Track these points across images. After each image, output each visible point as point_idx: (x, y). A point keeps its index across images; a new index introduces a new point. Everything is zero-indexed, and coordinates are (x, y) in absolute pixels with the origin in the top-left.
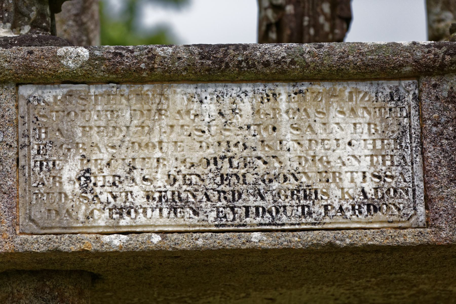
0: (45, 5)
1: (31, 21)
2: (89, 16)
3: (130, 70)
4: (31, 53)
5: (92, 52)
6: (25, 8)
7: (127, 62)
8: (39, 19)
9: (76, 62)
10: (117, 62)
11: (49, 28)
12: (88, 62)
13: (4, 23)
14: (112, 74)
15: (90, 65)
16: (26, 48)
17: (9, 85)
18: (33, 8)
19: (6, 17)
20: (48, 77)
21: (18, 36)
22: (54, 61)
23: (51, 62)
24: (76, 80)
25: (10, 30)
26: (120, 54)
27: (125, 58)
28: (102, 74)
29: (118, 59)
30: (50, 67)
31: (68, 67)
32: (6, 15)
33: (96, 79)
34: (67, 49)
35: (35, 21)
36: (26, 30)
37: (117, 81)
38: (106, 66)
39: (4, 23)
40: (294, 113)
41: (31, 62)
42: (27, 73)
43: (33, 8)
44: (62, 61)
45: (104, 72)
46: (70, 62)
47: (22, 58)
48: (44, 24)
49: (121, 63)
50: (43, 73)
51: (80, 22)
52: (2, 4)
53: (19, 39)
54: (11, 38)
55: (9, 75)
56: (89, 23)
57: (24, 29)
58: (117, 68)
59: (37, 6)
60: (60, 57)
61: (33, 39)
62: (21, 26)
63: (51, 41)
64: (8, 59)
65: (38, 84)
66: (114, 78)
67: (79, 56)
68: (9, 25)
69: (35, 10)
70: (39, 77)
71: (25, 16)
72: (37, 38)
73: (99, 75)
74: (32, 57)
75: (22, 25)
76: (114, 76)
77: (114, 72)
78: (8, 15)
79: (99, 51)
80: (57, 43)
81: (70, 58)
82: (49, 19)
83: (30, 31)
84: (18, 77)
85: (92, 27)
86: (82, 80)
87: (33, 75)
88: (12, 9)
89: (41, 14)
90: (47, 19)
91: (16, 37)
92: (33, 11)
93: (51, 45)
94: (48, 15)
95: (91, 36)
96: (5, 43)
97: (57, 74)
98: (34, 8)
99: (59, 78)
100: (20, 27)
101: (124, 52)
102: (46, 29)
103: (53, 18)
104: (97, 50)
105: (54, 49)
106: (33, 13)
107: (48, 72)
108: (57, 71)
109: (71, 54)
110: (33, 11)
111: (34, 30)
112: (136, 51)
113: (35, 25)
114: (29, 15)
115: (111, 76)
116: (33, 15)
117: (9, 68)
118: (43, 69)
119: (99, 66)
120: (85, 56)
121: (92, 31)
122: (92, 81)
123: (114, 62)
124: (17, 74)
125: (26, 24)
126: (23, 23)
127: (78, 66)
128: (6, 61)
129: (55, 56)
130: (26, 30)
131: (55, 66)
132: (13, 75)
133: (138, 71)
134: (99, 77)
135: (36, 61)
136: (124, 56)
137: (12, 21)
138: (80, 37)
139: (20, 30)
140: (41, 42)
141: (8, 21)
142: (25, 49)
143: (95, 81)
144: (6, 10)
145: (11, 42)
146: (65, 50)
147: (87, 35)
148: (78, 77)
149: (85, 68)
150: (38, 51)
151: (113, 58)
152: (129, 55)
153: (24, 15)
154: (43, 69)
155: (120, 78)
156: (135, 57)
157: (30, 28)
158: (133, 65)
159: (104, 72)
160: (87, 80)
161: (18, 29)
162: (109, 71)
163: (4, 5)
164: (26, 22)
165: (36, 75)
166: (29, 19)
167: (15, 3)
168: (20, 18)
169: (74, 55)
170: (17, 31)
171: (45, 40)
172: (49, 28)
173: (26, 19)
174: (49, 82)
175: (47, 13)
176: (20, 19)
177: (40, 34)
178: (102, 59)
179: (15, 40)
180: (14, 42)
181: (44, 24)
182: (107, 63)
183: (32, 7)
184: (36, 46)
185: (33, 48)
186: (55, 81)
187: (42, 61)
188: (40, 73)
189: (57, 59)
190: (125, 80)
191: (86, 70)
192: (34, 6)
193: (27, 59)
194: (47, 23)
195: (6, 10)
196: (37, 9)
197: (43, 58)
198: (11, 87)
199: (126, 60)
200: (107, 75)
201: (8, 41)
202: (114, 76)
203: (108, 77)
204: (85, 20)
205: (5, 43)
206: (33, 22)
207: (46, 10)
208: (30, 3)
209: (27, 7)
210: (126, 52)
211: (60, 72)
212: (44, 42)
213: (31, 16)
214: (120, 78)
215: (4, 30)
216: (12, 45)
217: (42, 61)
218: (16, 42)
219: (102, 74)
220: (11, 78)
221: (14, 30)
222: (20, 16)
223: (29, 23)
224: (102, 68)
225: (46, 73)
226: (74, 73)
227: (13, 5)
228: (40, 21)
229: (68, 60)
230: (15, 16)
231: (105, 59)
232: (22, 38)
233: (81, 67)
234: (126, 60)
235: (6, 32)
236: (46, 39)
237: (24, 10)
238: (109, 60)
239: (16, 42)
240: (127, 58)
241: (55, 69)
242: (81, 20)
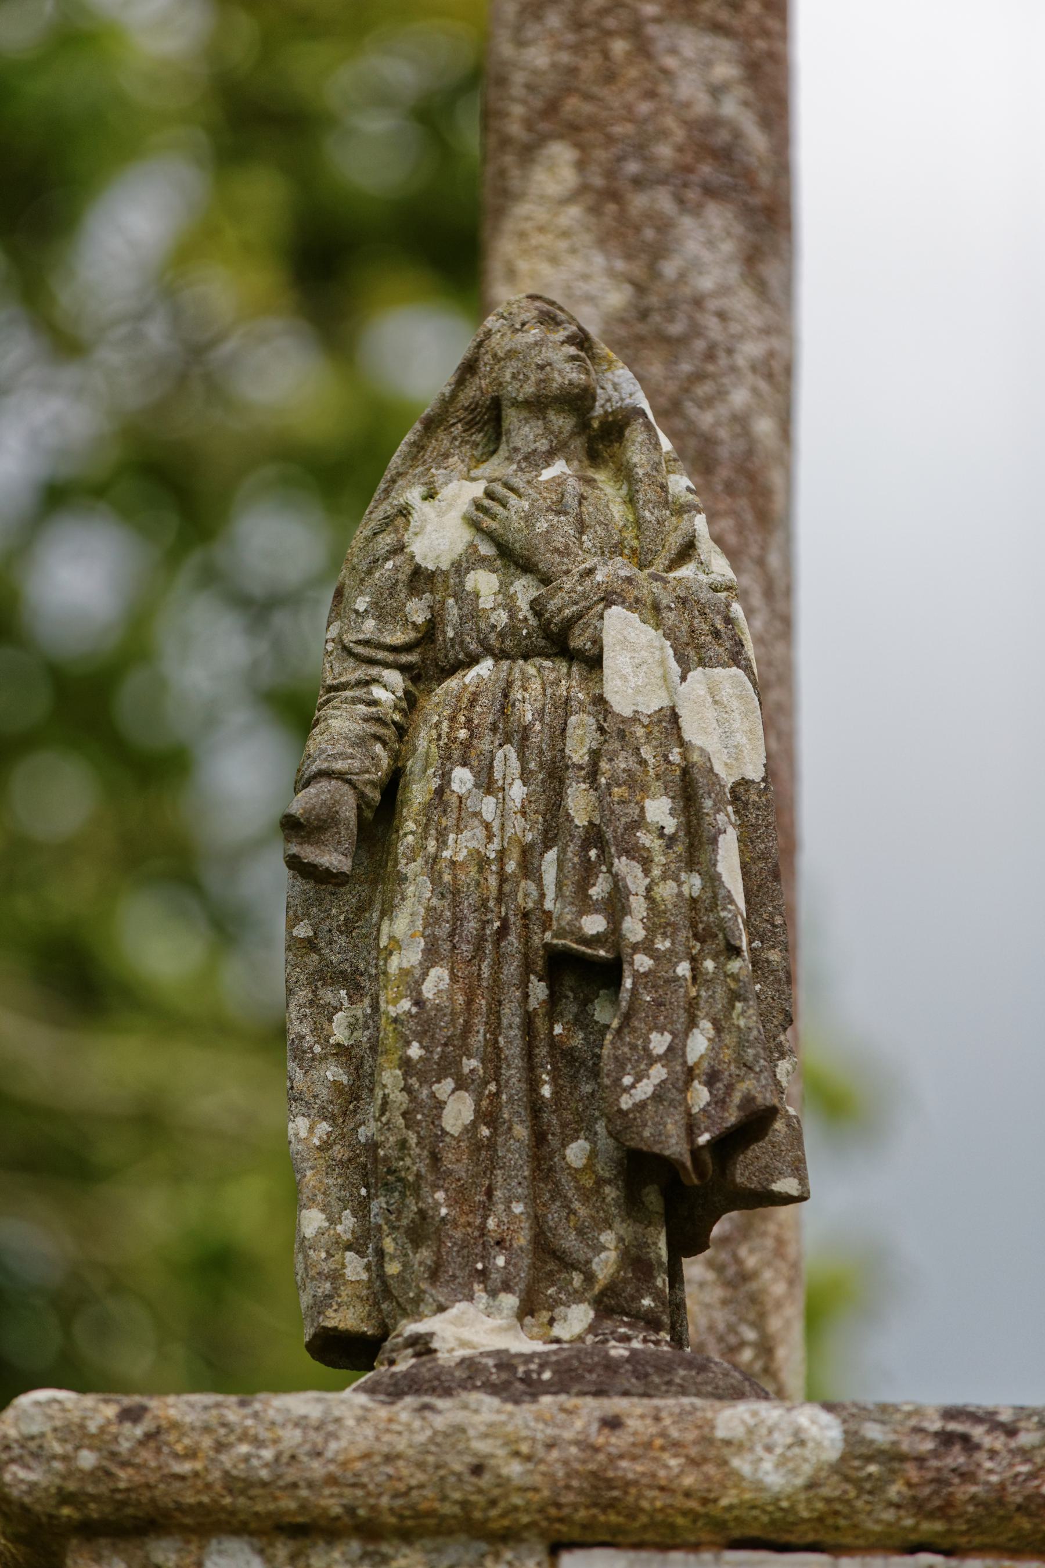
0: (650, 1224)
1: (597, 1289)
2: (770, 1243)
3: (1001, 1502)
4: (612, 1423)
5: (852, 1426)
6: (573, 1236)
7: (993, 1472)
8: (625, 1281)
9: (791, 1465)
10: (954, 1470)
11: (665, 1319)
12: (840, 1469)
13: (493, 1294)
14: (931, 1516)
15: (847, 1479)
16: (590, 1401)
17: (523, 1548)
18: (603, 1238)
19: (498, 1269)
20: (680, 1521)
21: (555, 1352)
22: (705, 1460)
23: (694, 1463)
24: (792, 1538)
25: (515, 1321)
26: (965, 1439)
27: (981, 1456)
28: (889, 1515)
29: (957, 1458)
30: (688, 1481)
31: (759, 1487)
32: (501, 1261)
33: (867, 1533)
34: (755, 1414)
35: (611, 1289)
36: (576, 1320)
37: (946, 1543)
38: (909, 1485)
39: (493, 1294)
40: (438, 455)
41: (612, 1459)
42: (595, 1505)
43: (603, 1238)
44: (736, 1462)
45: (898, 1506)
46: (767, 1465)
47: (577, 1443)
48: (647, 1302)
49: (967, 1476)
50: (659, 1504)
51: (731, 1271)
52: (485, 1218)
53: (557, 1362)
54: (528, 1358)
55: (527, 1511)
56: (767, 1274)
57: (565, 1319)
58: (951, 1494)
59: (621, 1228)
60: (728, 1443)
61: (611, 1366)
62: (553, 1304)
63: (682, 1372)
64: (524, 1448)
65: (638, 1546)
66: (937, 1534)
67: (802, 1443)
68: (510, 1301)
69: (612, 1246)
70: (644, 1519)
71: (573, 1267)
72: (628, 1360)
73: (878, 1521)
74: (618, 1441)
75: (558, 1302)
76: (939, 1526)
77: (940, 1508)
78: (507, 1262)
79: (883, 1423)
80: (706, 1383)
81: (769, 1449)
82: (661, 1281)
83: (592, 1329)
84: (561, 1520)
85: (779, 1289)
86: (811, 1537)
87: (618, 1513)
88: (522, 1240)
89: (636, 1262)
90: (659, 1283)
91: (547, 1354)
92: (604, 1248)
93: (684, 1392)
94: (661, 1264)
95: (775, 1324)
96: (504, 1376)
97: (713, 1510)
98: (608, 1238)
99: (718, 1525)
100: (551, 1309)
101: (977, 1432)
102: (652, 1323)
103: (676, 1277)
104: (875, 1421)
105: (703, 1410)
106: (603, 1255)
107: (679, 1501)
108: (715, 1501)
109: (770, 1432)
110: (604, 1248)
111: (608, 1324)
112: (1028, 1430)
113: (610, 1305)
114: (589, 1262)
115: (926, 1526)
116: (605, 1264)
117: (528, 1481)
118: (662, 1489)
119: (875, 1487)
120: (826, 1443)
121: (779, 1305)
122: (848, 1540)
123: (939, 1470)
124: (558, 1506)
125: (577, 1297)
126: (563, 1296)
127: (799, 1481)
128: (517, 1454)
129: (707, 1440)
130: (576, 1320)
131: (708, 1478)
132: (541, 1510)
133: (1033, 1507)
134: (878, 1528)
135: (634, 1458)
136: (978, 1447)
137: (522, 1286)
138: (732, 1329)
139: (552, 1321)
140: (646, 1377)
141: (507, 1287)
142: (590, 1409)
143: (861, 1542)
144: (498, 1243)
145: (528, 1373)
146: (747, 1417)
147: (759, 1323)
148: (794, 1524)
149: (826, 1491)
150: (642, 1417)
151: (935, 1454)
152: (998, 1445)
153: (566, 1262)
154: (662, 1489)
155: (963, 1533)
156: (1025, 1454)
157: (592, 1314)
158: (1014, 1484)
159: (898, 1506)
160: (829, 1538)
161: (545, 1316)
162: (917, 1506)
163: (491, 1223)
164: (576, 1291)
165: (632, 1513)
166: (590, 1278)
167: (536, 1217)
168: (551, 1273)
169: (782, 1439)
170: (542, 1325)
171: (660, 1370)
172: (665, 1319)
173: (577, 1279)
174: (678, 1541)
175: (660, 1257)
176: (550, 1278)
177: (636, 1344)
178: (892, 1457)
179: (542, 1367)
180: (539, 1374)
181: (647, 1302)
182: (912, 1472)
183: (601, 1230)
184: (626, 1394)
185: (617, 1404)
186: (705, 1537)
187: (655, 1459)
188: (645, 1504)
189: (710, 1451)
190: (977, 1540)
191: (828, 1501)
192: (610, 1227)
193: (596, 1449)
194: (657, 1296)
195: (498, 1243)
196: (621, 1239)
197: (663, 1449)
198: (531, 1556)
199: (988, 1465)
200: (909, 1522)
201: (513, 1368)
202: (939, 1526)
203: (914, 1529)
204: (751, 1262)
205: (504, 1376)
206: (603, 1293)
207: (655, 1244)
208: (592, 1217)
209: (580, 1232)
210: (989, 1432)
211: (724, 1502)
212: (656, 1380)
213: (594, 1267)
214: (963, 1533)
215: (491, 1323)
216: (533, 1389)
217: (655, 1459)
218: (547, 1375)
219: (889, 1515)
220: (533, 1524)
221: (528, 1320)
222: (552, 1266)
223: (588, 1295)
224: (895, 1490)
225: (671, 1506)
226: (782, 1509)
227: (526, 1225)
228: (629, 1290)
229: (761, 1459)
230: (533, 1266)
231: (903, 1458)
232: (571, 1357)
233: (811, 1485)
234: (988, 1465)
235: (501, 1330)
236: (665, 1367)
237: (570, 1242)
238: (920, 1460)
239: (547, 1375)
240: (993, 1454)
241: (709, 1491)
242: (738, 1261)
